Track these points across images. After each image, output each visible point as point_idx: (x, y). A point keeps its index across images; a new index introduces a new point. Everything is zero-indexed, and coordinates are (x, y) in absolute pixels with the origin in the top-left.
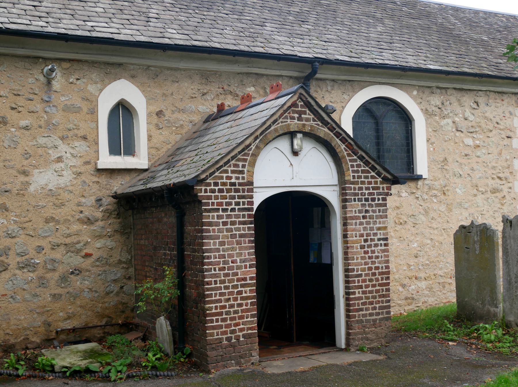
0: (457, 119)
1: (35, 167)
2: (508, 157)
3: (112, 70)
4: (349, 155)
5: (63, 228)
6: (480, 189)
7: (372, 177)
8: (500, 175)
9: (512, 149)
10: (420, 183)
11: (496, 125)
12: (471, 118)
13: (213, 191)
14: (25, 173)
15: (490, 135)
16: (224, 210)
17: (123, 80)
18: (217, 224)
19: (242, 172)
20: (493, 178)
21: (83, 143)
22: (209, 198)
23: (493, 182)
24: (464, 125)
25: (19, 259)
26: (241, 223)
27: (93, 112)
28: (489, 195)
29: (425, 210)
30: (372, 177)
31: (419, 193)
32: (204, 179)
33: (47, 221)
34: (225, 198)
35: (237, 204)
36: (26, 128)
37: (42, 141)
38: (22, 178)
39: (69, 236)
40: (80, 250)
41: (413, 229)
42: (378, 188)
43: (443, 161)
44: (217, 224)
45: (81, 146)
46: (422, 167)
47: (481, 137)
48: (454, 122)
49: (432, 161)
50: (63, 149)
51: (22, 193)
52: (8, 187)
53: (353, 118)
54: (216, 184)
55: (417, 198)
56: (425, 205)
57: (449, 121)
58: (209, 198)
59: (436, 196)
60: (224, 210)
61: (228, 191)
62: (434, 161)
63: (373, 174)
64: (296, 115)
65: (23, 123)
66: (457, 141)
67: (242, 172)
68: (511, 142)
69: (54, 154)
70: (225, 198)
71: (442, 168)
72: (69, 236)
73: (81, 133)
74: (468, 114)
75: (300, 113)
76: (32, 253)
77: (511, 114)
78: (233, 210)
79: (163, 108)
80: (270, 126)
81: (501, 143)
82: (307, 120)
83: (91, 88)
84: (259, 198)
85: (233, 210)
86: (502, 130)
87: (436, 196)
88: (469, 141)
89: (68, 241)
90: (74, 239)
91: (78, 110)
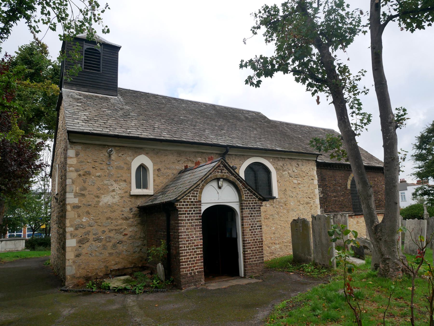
1: (103, 194)
3: (138, 151)
4: (243, 188)
7: (254, 198)
10: (275, 200)
12: (296, 171)
13: (183, 205)
14: (98, 197)
15: (304, 178)
19: (196, 196)
21: (124, 183)
22: (182, 208)
25: (94, 236)
26: (196, 219)
27: (129, 169)
28: (305, 205)
30: (254, 198)
31: (274, 205)
33: (107, 219)
35: (194, 211)
36: (99, 176)
38: (97, 199)
40: (122, 232)
42: (257, 203)
45: (123, 185)
46: (275, 193)
49: (280, 190)
50: (115, 186)
52: (90, 203)
54: (184, 202)
55: (274, 207)
57: (287, 172)
58: (182, 208)
59: (282, 206)
63: (254, 197)
64: (220, 171)
65: (98, 174)
67: (196, 196)
69: (111, 188)
72: (117, 225)
73: (123, 179)
74: (294, 169)
75: (222, 170)
76: (100, 233)
77: (313, 169)
79: (160, 167)
80: (208, 176)
82: (225, 173)
83: (129, 159)
84: (204, 208)
87: (282, 206)
88: (295, 181)
89: (117, 228)
90: (120, 227)
91: (122, 168)
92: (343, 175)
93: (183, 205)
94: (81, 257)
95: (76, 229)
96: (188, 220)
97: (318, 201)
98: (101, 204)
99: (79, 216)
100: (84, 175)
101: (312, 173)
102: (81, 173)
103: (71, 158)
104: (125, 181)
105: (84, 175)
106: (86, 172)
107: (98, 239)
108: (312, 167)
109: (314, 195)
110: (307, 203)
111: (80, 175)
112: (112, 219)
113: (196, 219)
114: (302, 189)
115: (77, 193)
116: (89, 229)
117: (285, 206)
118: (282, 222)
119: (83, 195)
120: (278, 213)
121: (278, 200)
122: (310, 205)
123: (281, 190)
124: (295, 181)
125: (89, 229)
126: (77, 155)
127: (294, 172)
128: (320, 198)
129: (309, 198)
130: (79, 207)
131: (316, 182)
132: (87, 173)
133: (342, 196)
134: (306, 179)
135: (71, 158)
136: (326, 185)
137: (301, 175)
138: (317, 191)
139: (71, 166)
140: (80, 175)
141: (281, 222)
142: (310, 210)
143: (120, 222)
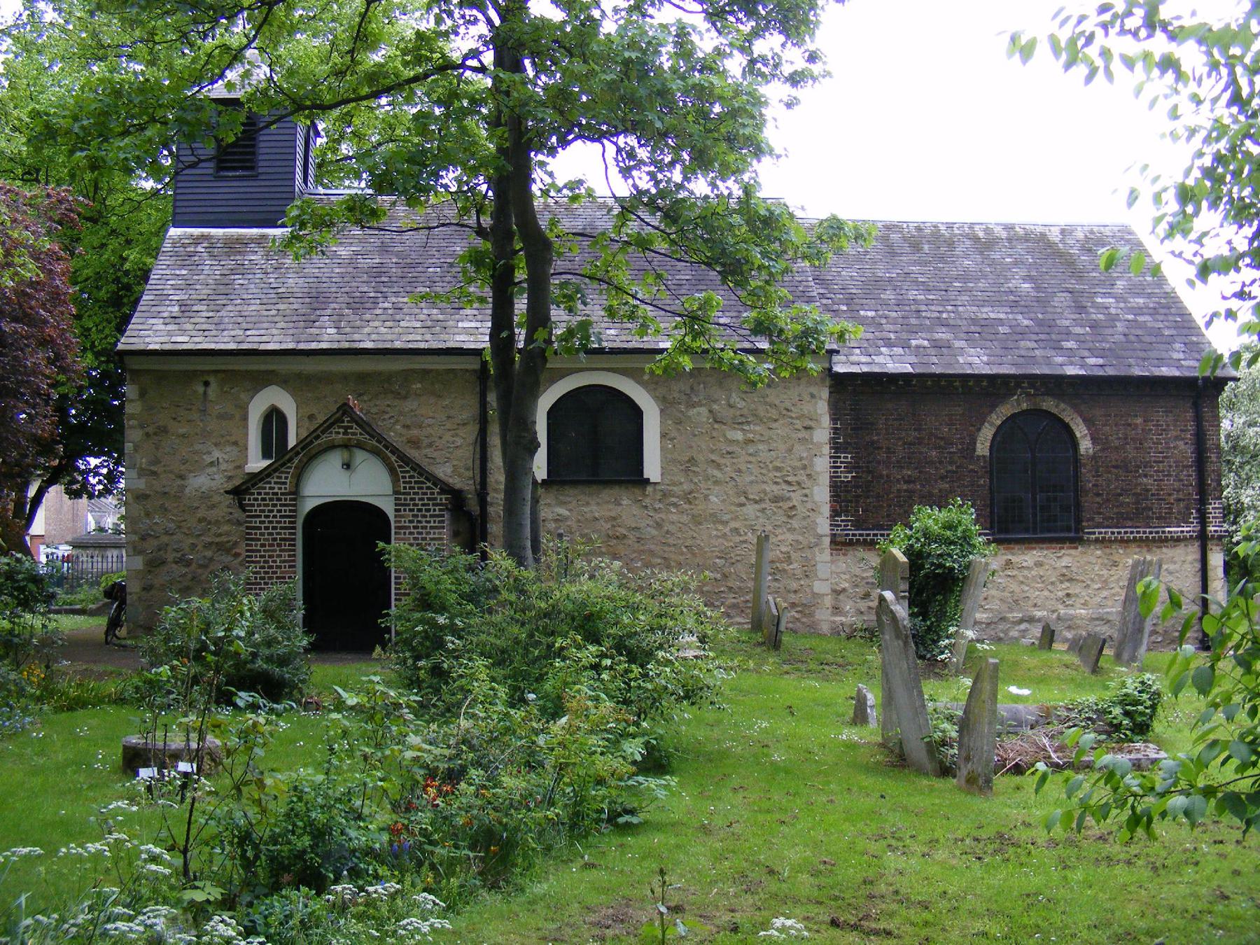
0: (715, 407)
1: (191, 471)
2: (805, 455)
3: (261, 381)
4: (400, 466)
5: (214, 529)
6: (751, 497)
7: (428, 488)
8: (789, 479)
9: (812, 443)
10: (649, 489)
11: (785, 412)
12: (741, 404)
13: (256, 500)
14: (182, 477)
15: (774, 425)
16: (267, 517)
17: (274, 387)
18: (260, 528)
19: (285, 483)
20: (776, 483)
21: (234, 448)
22: (253, 505)
23: (775, 488)
24: (727, 414)
25: (175, 554)
26: (282, 528)
27: (245, 418)
28: (767, 505)
29: (657, 523)
30: (428, 488)
31: (647, 501)
32: (248, 489)
33: (200, 521)
34: (267, 505)
35: (279, 511)
36: (183, 436)
37: (198, 447)
38: (179, 482)
39: (220, 535)
40: (231, 549)
41: (636, 545)
42: (435, 499)
43: (689, 461)
44: (260, 528)
45: (232, 451)
46: (652, 468)
47: (757, 428)
48: (710, 411)
49: (667, 462)
50: (217, 454)
51: (177, 498)
52: (167, 490)
53: (549, 413)
54: (259, 494)
55: (646, 507)
56: (657, 516)
57: (703, 410)
58: (253, 505)
59: (675, 505)
60: (267, 517)
61: (271, 499)
62: (674, 461)
63: (429, 484)
64: (341, 430)
65: (181, 431)
66: (715, 434)
67: (285, 483)
68: (811, 436)
69: (208, 459)
70: (267, 505)
71: (687, 470)
72: (220, 535)
73: (233, 439)
74: (735, 399)
75: (346, 428)
76: (187, 550)
77: (813, 396)
78: (275, 516)
79: (315, 411)
80: (311, 442)
81: (794, 436)
82: (353, 434)
83: (242, 396)
84: (310, 505)
85: (275, 516)
86: (797, 418)
87: (675, 505)
88: (739, 436)
89: (217, 540)
90: (224, 539)
91: (231, 417)
92: (960, 410)
93: (256, 500)
94: (152, 592)
95: (143, 538)
96: (267, 528)
97: (822, 494)
98: (187, 491)
99: (148, 515)
100: (155, 434)
101: (806, 408)
102: (150, 430)
103: (132, 401)
104: (235, 443)
105: (155, 434)
106: (159, 428)
107: (182, 561)
108: (814, 390)
109: (809, 476)
110: (776, 499)
111: (147, 435)
112: (210, 523)
113: (282, 528)
114: (764, 456)
115: (143, 469)
116: (165, 539)
117: (686, 506)
118: (673, 549)
119: (154, 473)
120: (659, 525)
121: (658, 487)
122: (786, 505)
123: (674, 461)
124: (739, 436)
125: (165, 539)
126: (143, 394)
127: (731, 406)
128: (837, 489)
129: (789, 483)
130: (146, 497)
131: (823, 434)
132: (163, 430)
133: (942, 478)
134: (780, 429)
135: (132, 401)
136: (873, 442)
137: (762, 414)
138: (822, 465)
139: (132, 417)
140: (147, 435)
141: (666, 548)
142: (784, 519)
143: (226, 528)
